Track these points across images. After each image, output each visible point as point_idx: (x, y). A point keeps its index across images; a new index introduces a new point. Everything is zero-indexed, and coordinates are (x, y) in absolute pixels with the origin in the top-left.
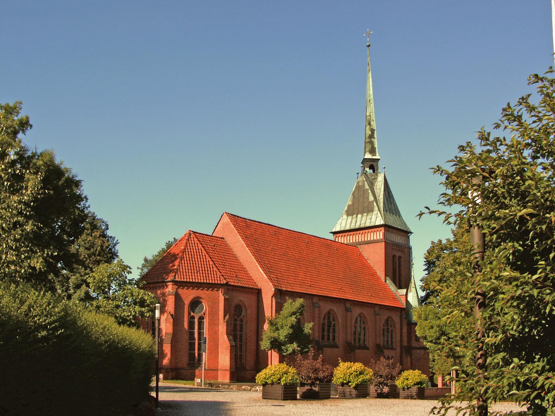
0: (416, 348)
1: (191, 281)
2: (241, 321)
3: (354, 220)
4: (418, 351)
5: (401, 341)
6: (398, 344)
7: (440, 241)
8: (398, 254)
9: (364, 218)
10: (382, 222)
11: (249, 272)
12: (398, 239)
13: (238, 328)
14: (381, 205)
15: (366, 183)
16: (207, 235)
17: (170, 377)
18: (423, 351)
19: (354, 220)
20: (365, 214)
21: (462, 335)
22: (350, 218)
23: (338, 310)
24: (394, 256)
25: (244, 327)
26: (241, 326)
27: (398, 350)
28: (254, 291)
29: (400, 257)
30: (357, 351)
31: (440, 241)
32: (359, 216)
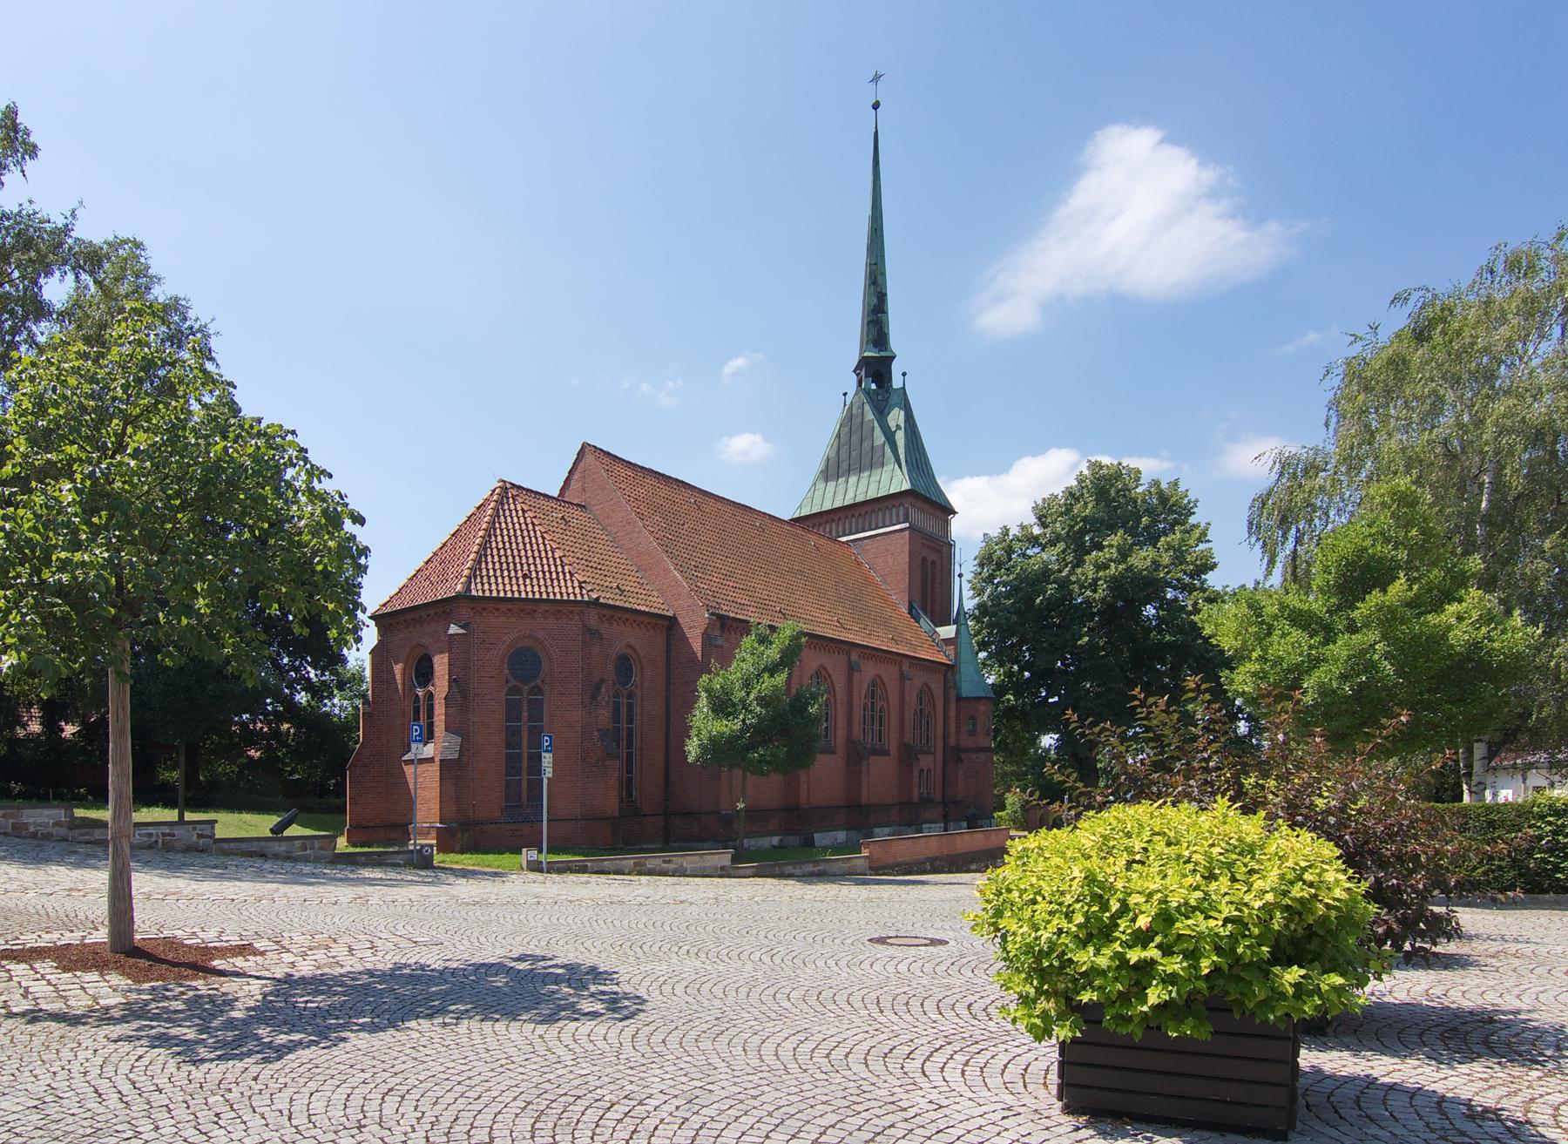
0: (970, 750)
1: (509, 595)
2: (630, 696)
3: (841, 488)
4: (974, 756)
5: (945, 736)
6: (940, 743)
7: (1006, 531)
8: (932, 556)
9: (863, 483)
10: (906, 486)
11: (433, 959)
12: (928, 524)
13: (624, 712)
14: (901, 451)
15: (867, 407)
16: (545, 496)
17: (457, 846)
18: (982, 755)
19: (841, 488)
20: (866, 474)
21: (727, 692)
22: (832, 484)
23: (889, 673)
24: (924, 559)
25: (637, 709)
26: (630, 707)
27: (940, 753)
28: (660, 622)
29: (933, 563)
30: (872, 758)
31: (1006, 531)
32: (853, 479)
